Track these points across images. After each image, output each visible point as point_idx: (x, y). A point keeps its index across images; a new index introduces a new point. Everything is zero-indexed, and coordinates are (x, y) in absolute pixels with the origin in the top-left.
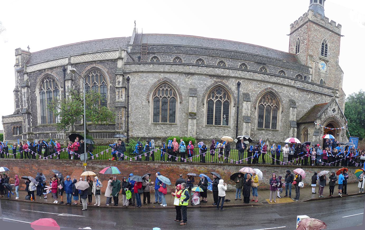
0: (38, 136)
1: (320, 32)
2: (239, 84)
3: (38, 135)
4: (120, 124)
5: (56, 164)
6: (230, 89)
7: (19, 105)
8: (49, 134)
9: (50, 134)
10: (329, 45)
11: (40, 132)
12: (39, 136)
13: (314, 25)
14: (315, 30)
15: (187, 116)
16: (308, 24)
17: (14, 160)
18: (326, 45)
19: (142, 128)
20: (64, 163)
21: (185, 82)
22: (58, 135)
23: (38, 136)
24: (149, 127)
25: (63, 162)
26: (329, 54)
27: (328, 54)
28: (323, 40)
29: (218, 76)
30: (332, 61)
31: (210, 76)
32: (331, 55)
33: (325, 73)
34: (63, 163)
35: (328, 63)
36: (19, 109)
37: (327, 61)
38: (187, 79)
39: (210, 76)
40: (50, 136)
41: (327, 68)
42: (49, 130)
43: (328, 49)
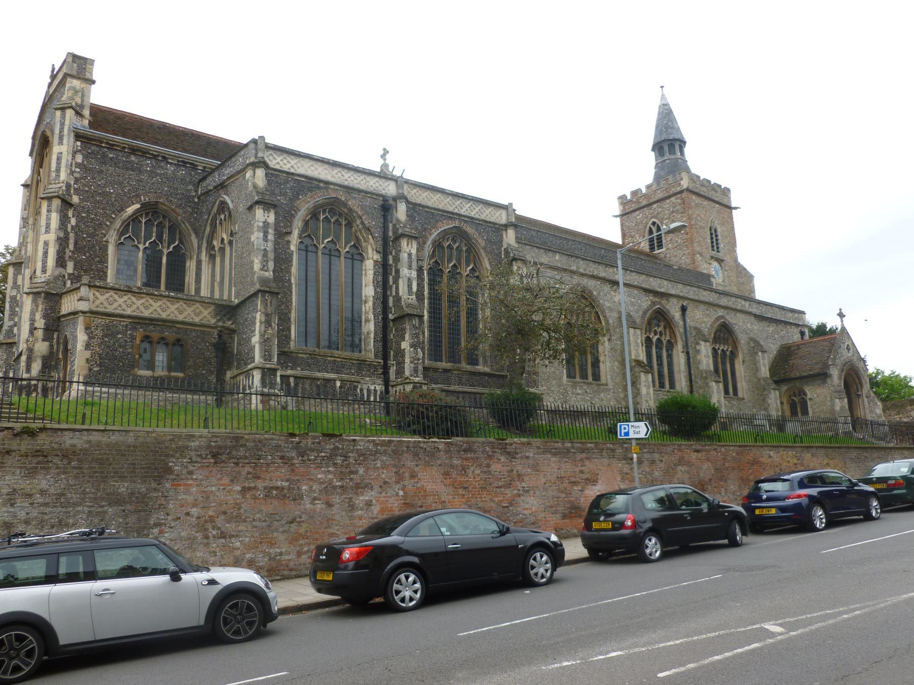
0: (292, 384)
1: (703, 208)
2: (684, 309)
3: (292, 380)
4: (532, 374)
5: (554, 454)
6: (673, 318)
7: (67, 258)
8: (335, 384)
9: (338, 384)
10: (719, 230)
11: (298, 372)
12: (296, 385)
13: (694, 197)
14: (697, 205)
15: (621, 368)
16: (684, 195)
17: (419, 442)
18: (716, 231)
19: (552, 389)
20: (576, 451)
21: (611, 298)
22: (361, 390)
23: (292, 384)
24: (564, 389)
25: (573, 448)
26: (722, 246)
27: (721, 246)
28: (710, 221)
29: (656, 293)
30: (727, 258)
31: (647, 291)
32: (725, 248)
33: (722, 283)
34: (572, 450)
35: (723, 265)
36: (64, 276)
37: (722, 261)
38: (613, 293)
39: (647, 291)
40: (338, 390)
41: (724, 273)
42: (332, 371)
43: (719, 237)
